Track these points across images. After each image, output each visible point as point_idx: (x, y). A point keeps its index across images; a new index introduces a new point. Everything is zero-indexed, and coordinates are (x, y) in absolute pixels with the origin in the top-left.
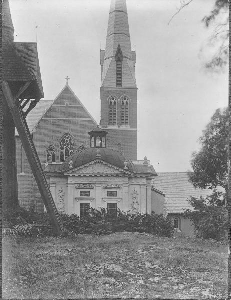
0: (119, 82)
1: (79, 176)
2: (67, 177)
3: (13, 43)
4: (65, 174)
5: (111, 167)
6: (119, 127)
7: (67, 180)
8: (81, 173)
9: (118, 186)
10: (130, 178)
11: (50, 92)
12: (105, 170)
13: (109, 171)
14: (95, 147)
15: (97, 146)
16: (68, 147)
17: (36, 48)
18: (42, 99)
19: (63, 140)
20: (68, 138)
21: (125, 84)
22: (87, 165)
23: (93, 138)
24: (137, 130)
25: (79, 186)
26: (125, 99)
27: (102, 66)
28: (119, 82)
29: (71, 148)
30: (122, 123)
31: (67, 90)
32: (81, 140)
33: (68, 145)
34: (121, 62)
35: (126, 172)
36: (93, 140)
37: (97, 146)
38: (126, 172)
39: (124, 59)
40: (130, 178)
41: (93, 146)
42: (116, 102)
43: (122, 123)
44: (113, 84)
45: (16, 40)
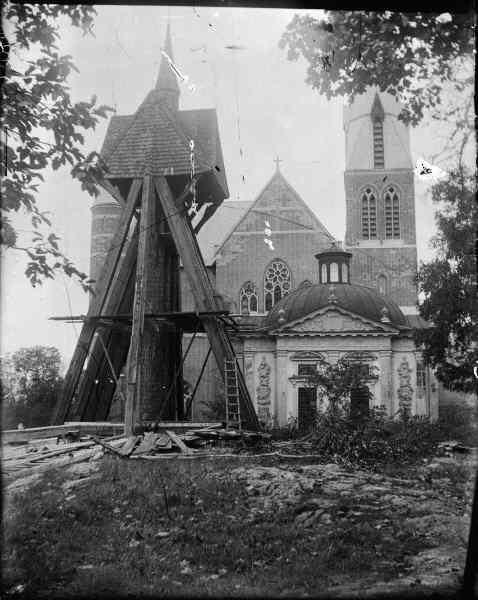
0: (379, 160)
1: (297, 337)
2: (274, 339)
3: (177, 114)
4: (271, 333)
5: (357, 319)
6: (382, 243)
7: (276, 343)
8: (300, 330)
9: (369, 355)
10: (394, 339)
11: (243, 185)
12: (348, 324)
13: (353, 326)
14: (329, 282)
15: (332, 280)
16: (281, 284)
17: (93, 231)
18: (225, 200)
19: (271, 270)
20: (281, 266)
21: (391, 162)
22: (311, 316)
23: (324, 267)
24: (415, 249)
25: (298, 356)
26: (392, 190)
27: (347, 132)
28: (379, 160)
29: (286, 286)
30: (387, 235)
31: (278, 176)
32: (305, 269)
33: (275, 280)
34: (381, 123)
35: (386, 329)
36: (324, 270)
37: (332, 280)
38: (386, 329)
39: (387, 116)
40: (394, 339)
41: (324, 280)
42: (398, 195)
43: (387, 235)
44: (368, 163)
45: (181, 109)
